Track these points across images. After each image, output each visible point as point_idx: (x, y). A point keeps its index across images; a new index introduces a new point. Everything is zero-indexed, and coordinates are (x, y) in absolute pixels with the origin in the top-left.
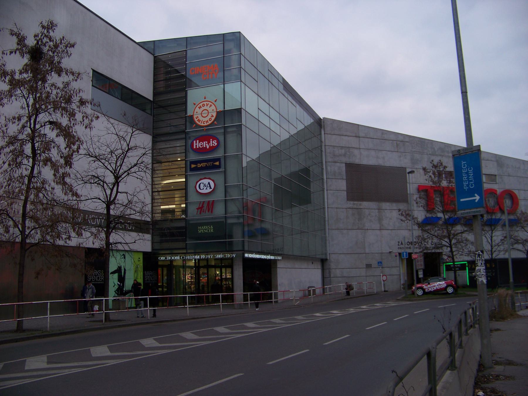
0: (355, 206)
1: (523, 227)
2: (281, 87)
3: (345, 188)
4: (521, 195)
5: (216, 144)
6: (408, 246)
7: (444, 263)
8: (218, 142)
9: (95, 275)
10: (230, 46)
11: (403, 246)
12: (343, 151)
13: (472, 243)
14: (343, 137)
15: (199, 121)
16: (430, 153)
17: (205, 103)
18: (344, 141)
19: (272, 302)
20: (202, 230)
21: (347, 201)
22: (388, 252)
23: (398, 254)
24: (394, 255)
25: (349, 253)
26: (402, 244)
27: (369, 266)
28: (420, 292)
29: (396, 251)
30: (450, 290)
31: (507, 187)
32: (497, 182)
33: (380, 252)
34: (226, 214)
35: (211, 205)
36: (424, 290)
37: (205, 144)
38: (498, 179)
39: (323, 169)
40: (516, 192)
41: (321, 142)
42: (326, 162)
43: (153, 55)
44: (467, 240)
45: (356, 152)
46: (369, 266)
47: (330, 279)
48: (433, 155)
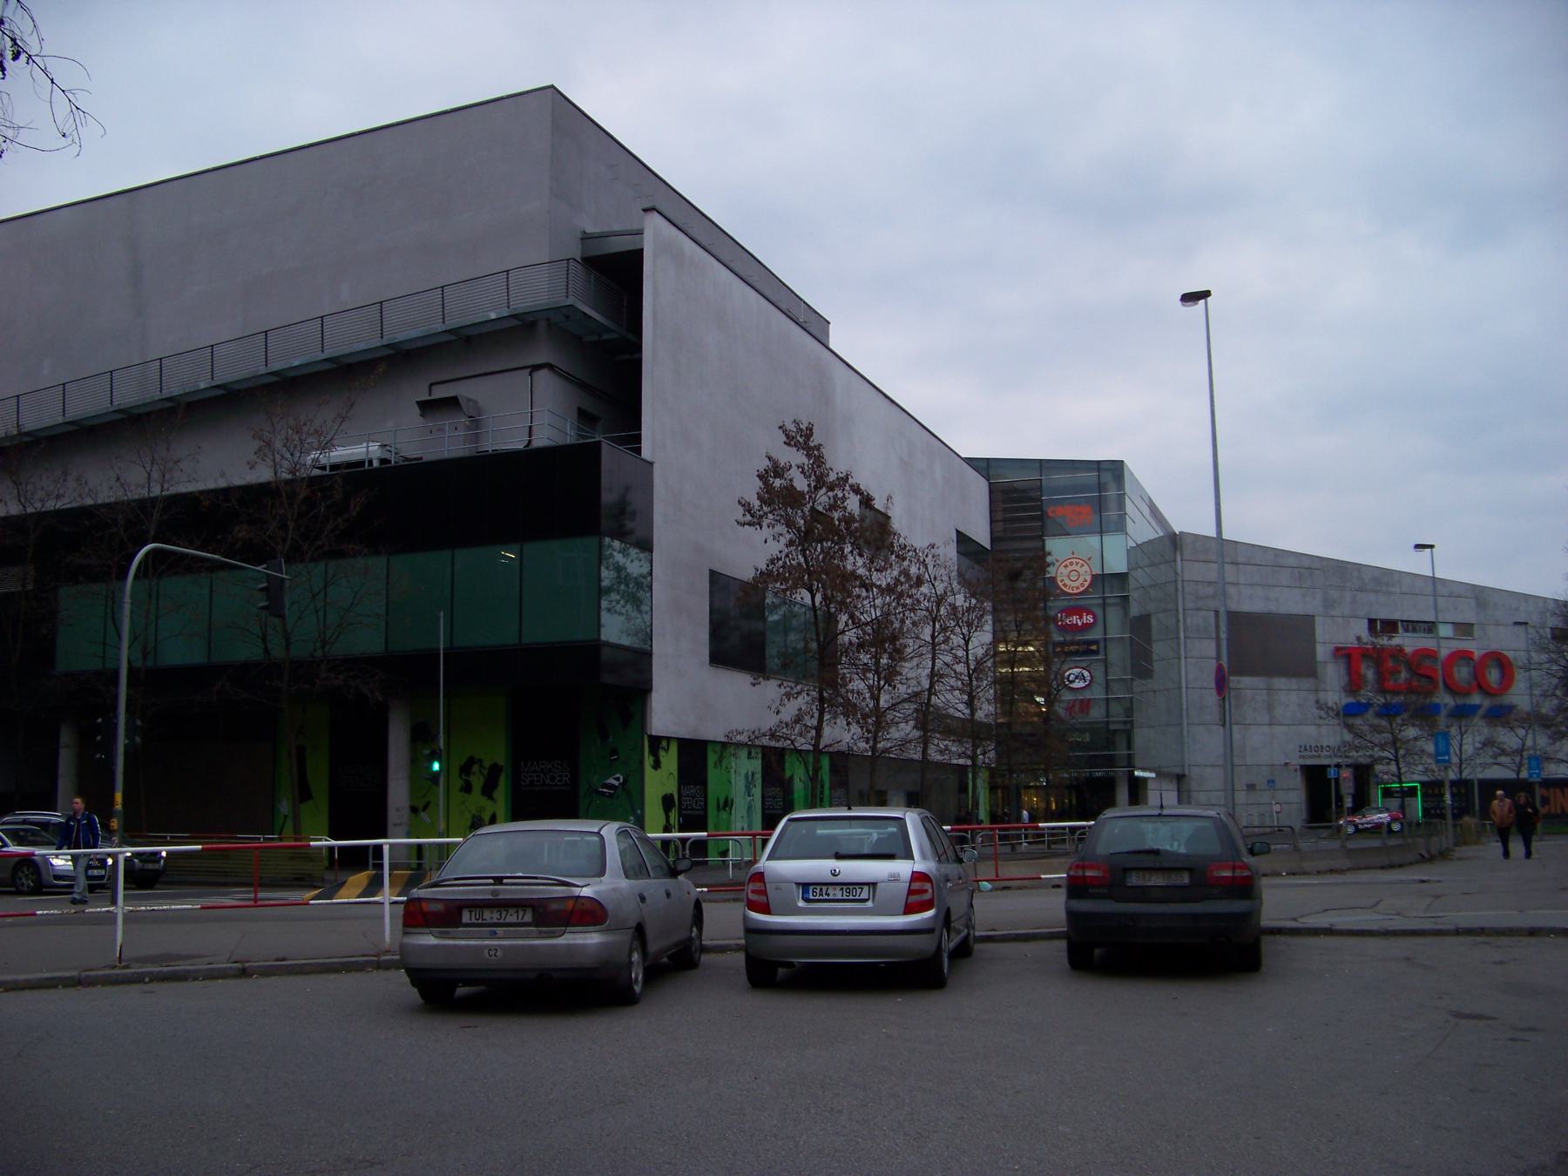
1: (1512, 729)
2: (1146, 511)
5: (1092, 620)
6: (1316, 754)
7: (1378, 784)
8: (1095, 617)
10: (1107, 477)
13: (1430, 755)
15: (1065, 585)
20: (1076, 738)
22: (1282, 763)
23: (1298, 767)
24: (1292, 768)
28: (1351, 830)
29: (1296, 761)
30: (1396, 827)
32: (1476, 636)
34: (1108, 716)
35: (1085, 705)
36: (1356, 826)
37: (1075, 619)
38: (1477, 631)
39: (1178, 621)
41: (1176, 574)
42: (1184, 610)
43: (988, 480)
44: (1423, 751)
45: (1231, 590)
48: (1360, 590)
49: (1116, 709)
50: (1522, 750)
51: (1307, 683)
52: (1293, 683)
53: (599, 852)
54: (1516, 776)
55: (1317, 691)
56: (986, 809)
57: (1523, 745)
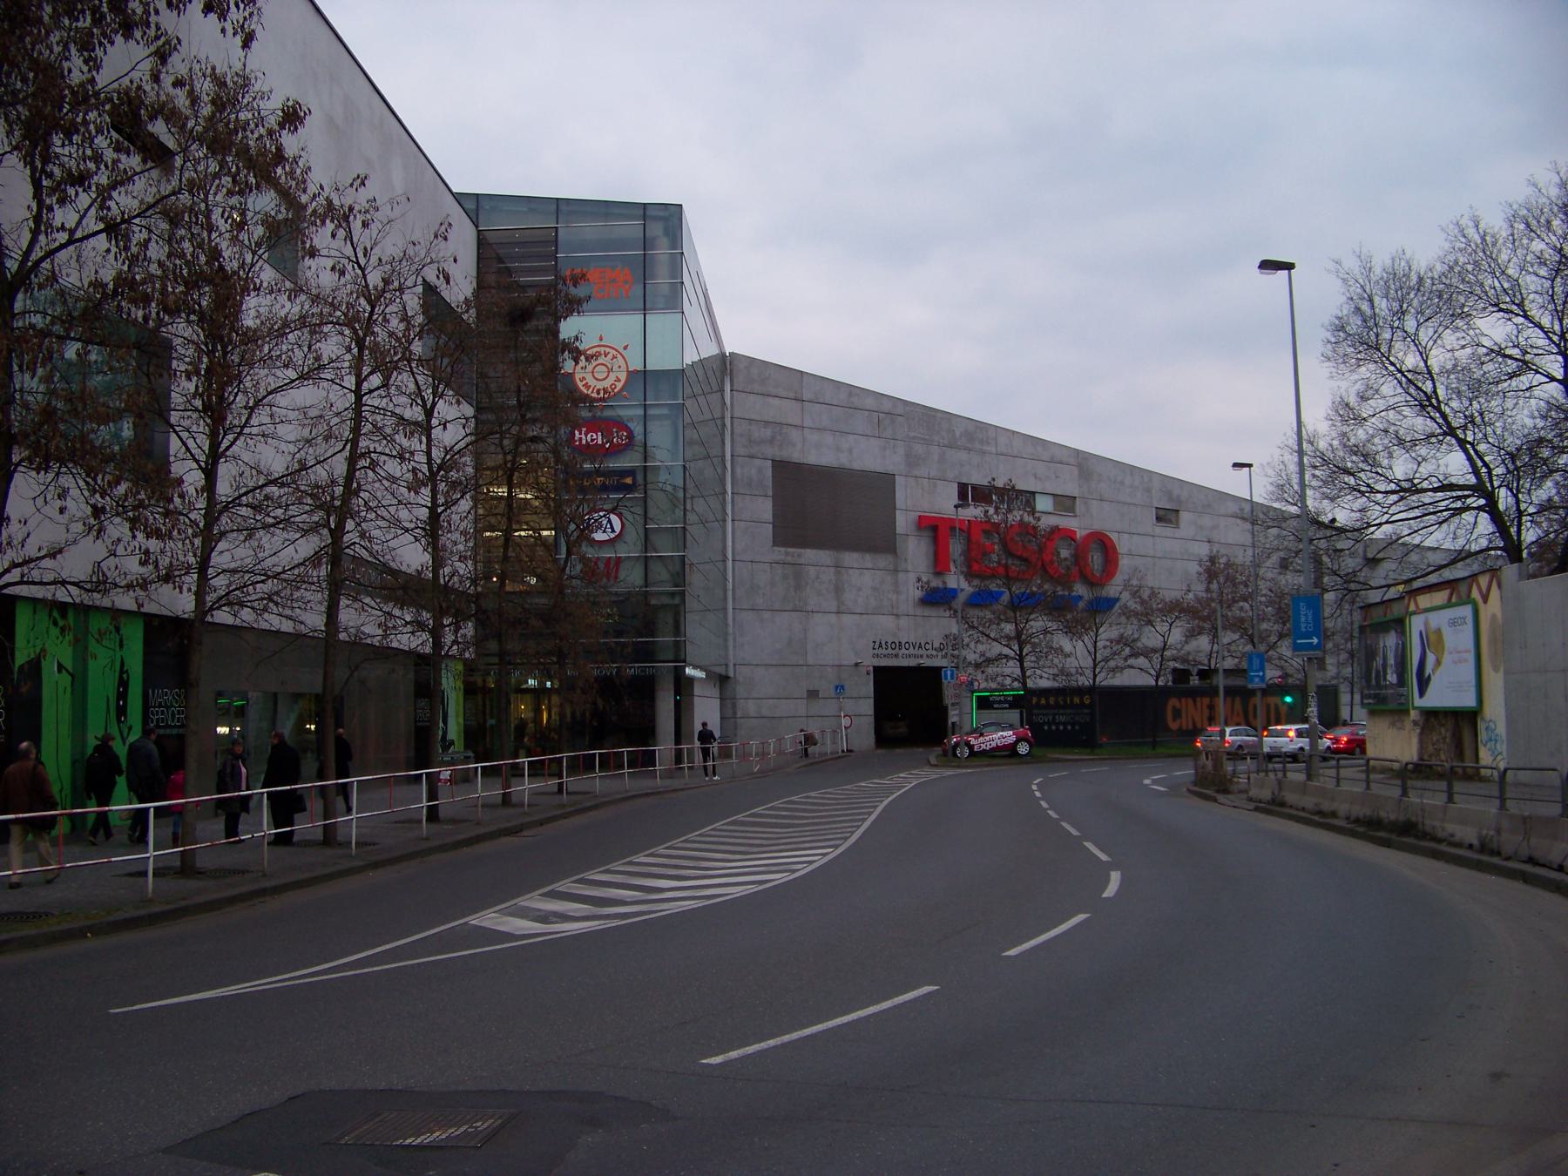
0: (789, 559)
3: (768, 516)
4: (1123, 544)
6: (893, 652)
9: (166, 707)
10: (656, 229)
11: (884, 652)
12: (768, 432)
14: (770, 400)
16: (946, 442)
17: (602, 349)
18: (776, 409)
19: (714, 766)
21: (773, 546)
22: (853, 662)
23: (871, 668)
24: (864, 671)
25: (774, 663)
26: (880, 646)
27: (813, 694)
29: (870, 662)
30: (1023, 749)
31: (1097, 526)
33: (836, 663)
36: (971, 747)
40: (1114, 536)
43: (477, 227)
45: (795, 435)
46: (813, 694)
47: (736, 722)
49: (661, 573)
50: (1164, 649)
51: (884, 561)
52: (868, 559)
54: (1154, 683)
55: (896, 571)
56: (458, 724)
57: (1165, 645)
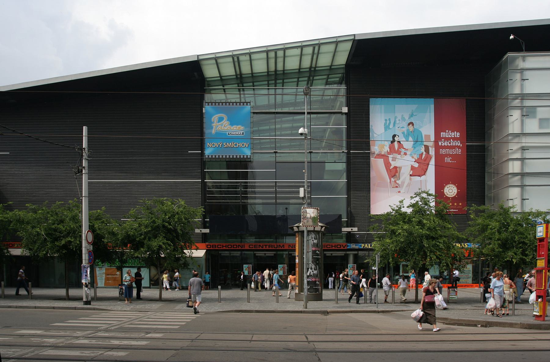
15: (447, 194)
53: (266, 57)
